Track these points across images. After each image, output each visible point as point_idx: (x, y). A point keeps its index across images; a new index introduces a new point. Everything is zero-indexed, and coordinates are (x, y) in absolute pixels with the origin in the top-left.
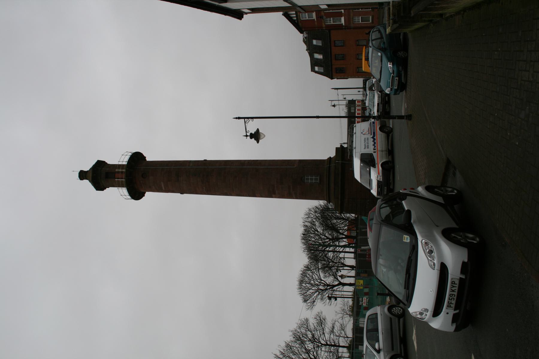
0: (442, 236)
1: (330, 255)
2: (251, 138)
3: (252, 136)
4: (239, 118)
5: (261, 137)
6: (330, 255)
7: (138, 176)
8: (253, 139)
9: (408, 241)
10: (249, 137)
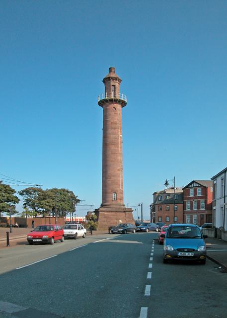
3: (167, 182)
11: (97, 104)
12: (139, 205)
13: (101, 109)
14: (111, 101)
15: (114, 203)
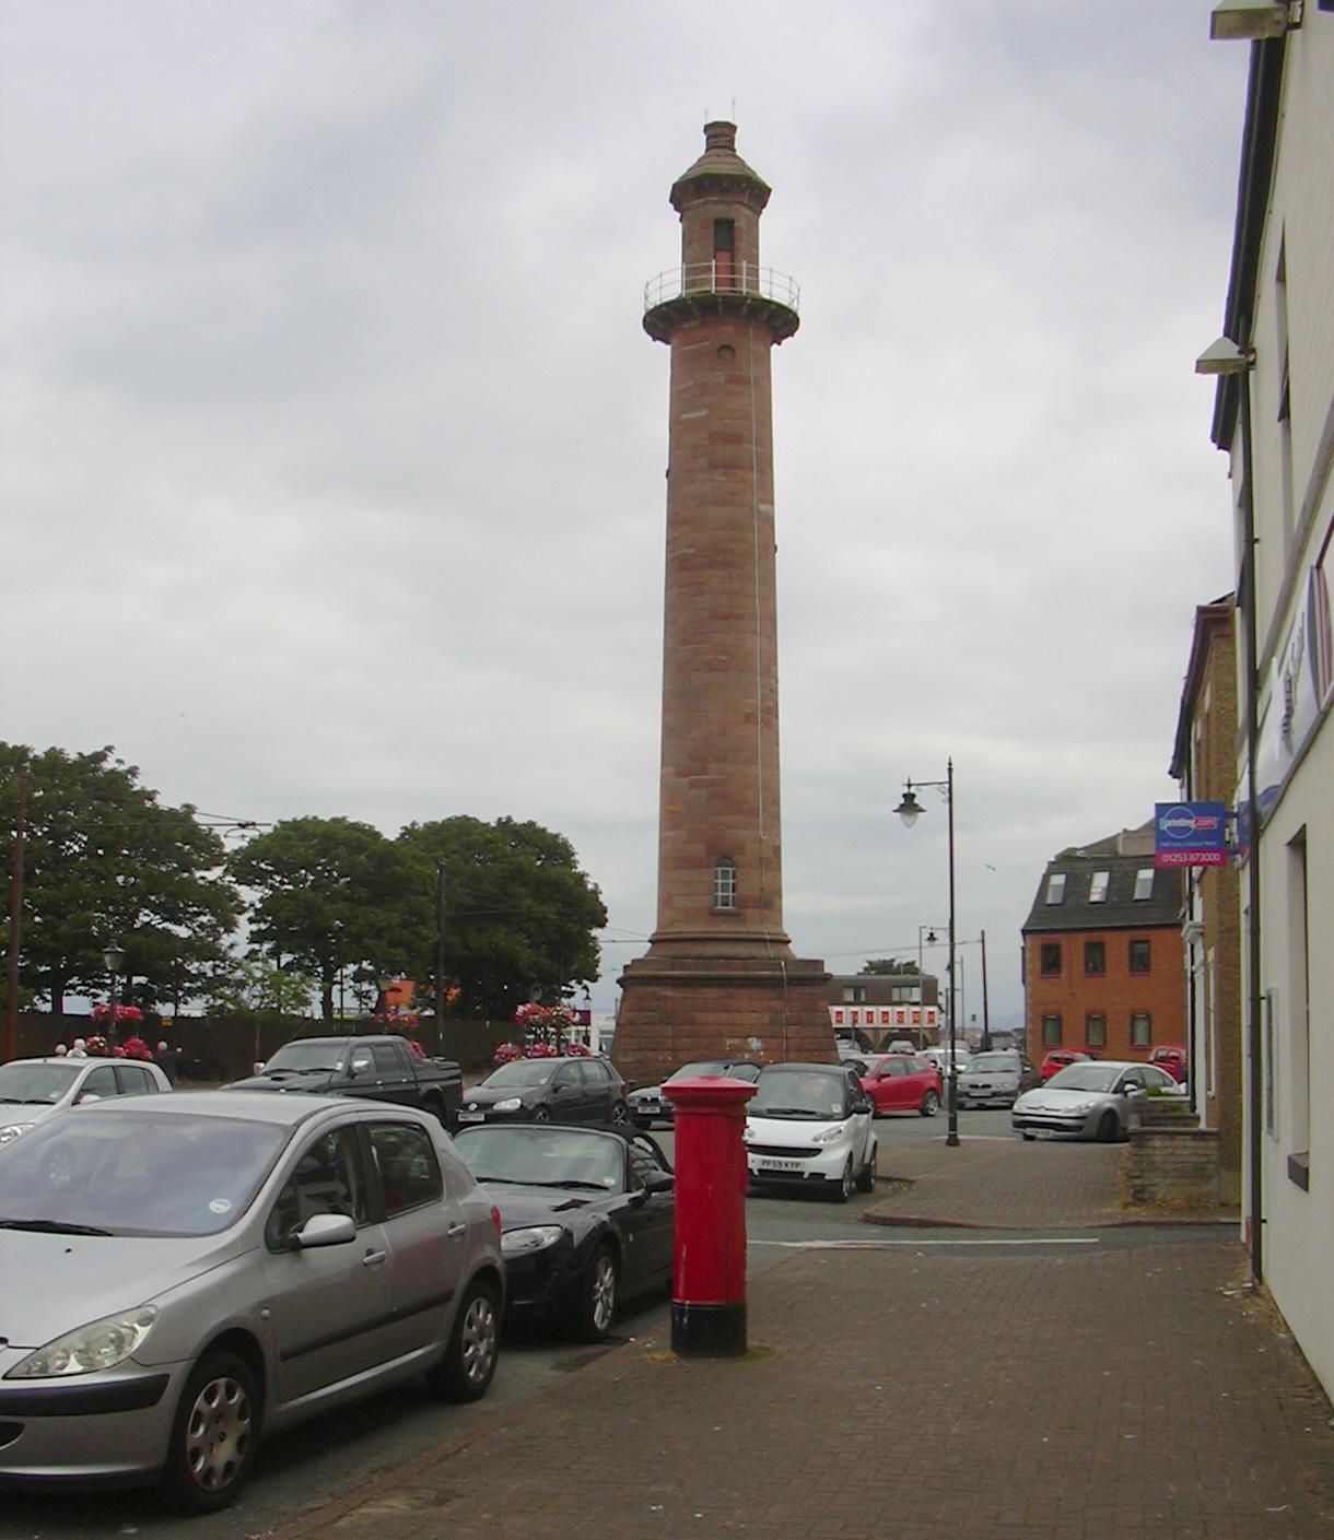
3: (909, 797)
4: (950, 770)
5: (906, 818)
7: (721, 327)
8: (902, 801)
9: (835, 1111)
10: (906, 791)
15: (725, 928)
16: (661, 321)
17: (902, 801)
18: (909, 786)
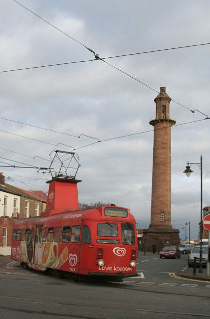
0: (62, 282)
1: (157, 242)
2: (187, 167)
3: (188, 167)
4: (201, 159)
6: (157, 242)
8: (186, 169)
10: (187, 165)
11: (188, 178)
12: (183, 228)
13: (152, 128)
14: (162, 121)
15: (162, 224)
16: (152, 123)
17: (186, 169)
18: (188, 164)
